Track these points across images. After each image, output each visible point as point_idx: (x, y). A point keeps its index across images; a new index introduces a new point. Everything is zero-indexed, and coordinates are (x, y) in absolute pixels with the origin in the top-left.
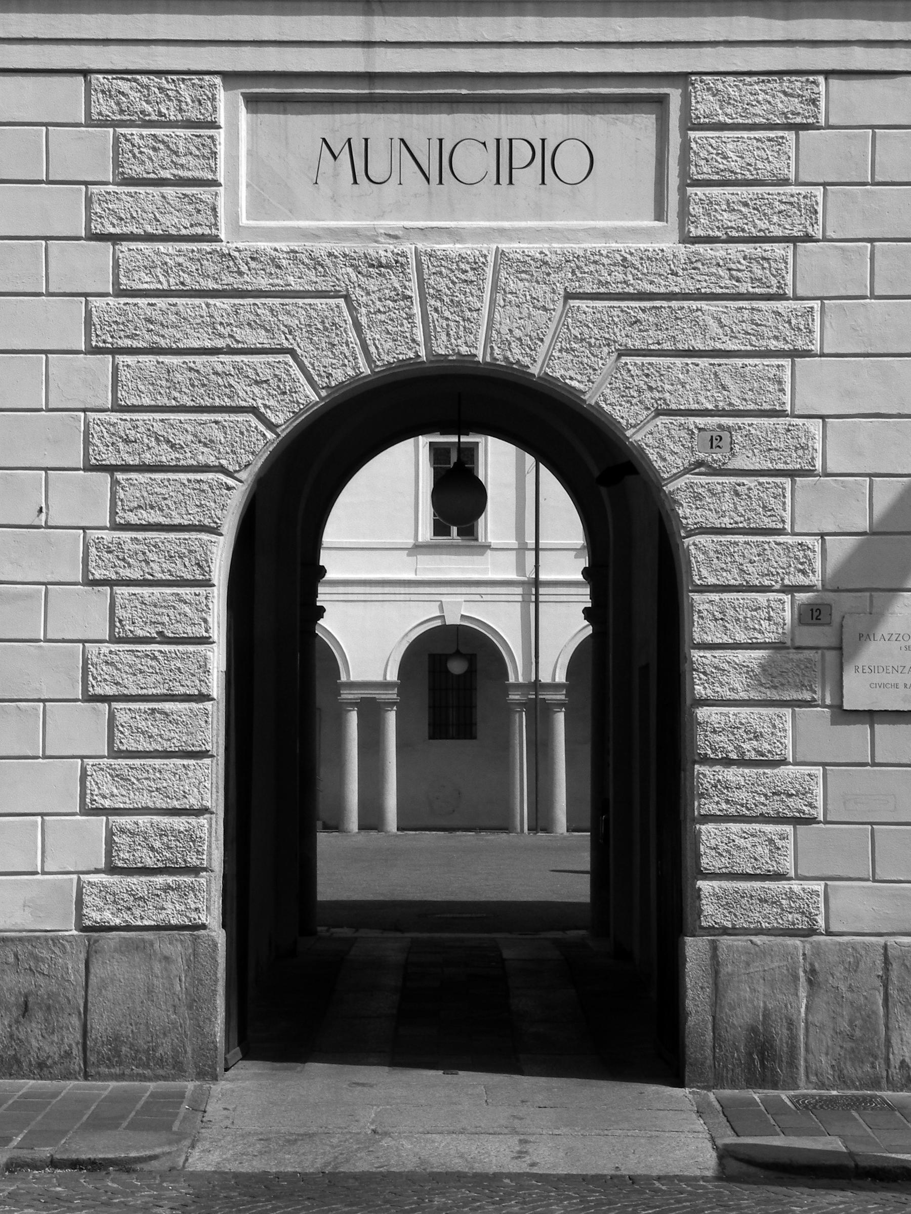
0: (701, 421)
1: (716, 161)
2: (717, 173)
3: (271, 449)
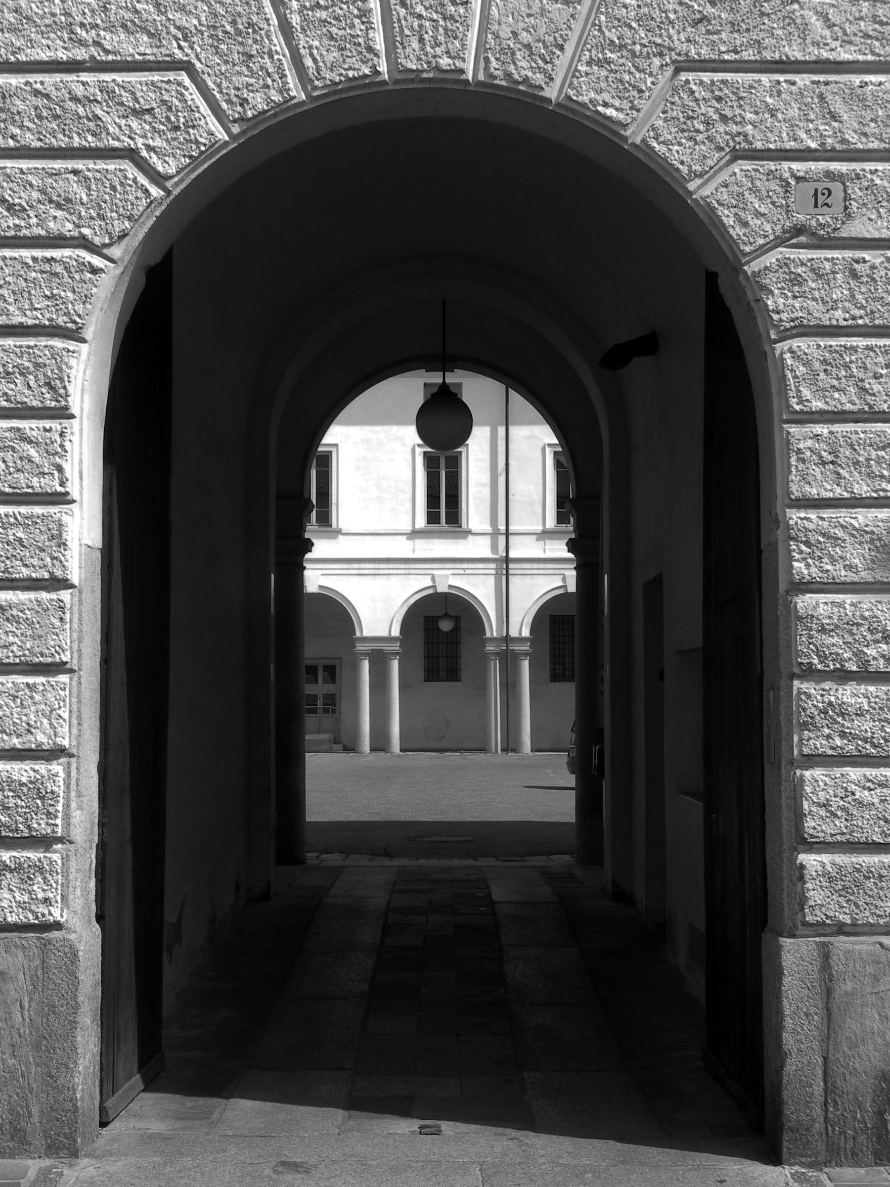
3: (158, 213)
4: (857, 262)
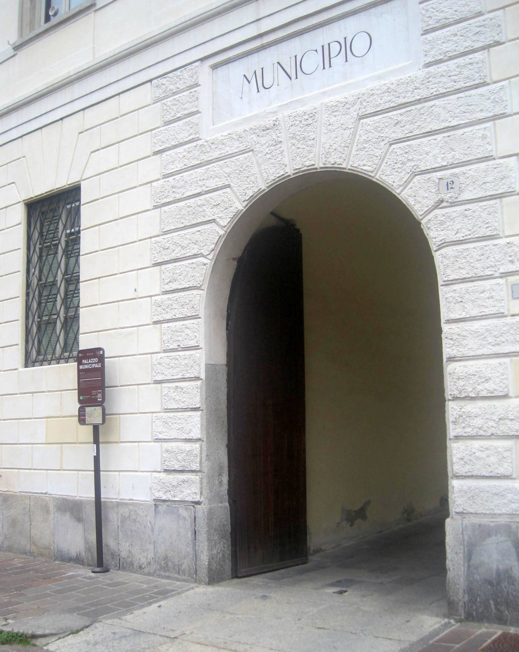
0: (439, 174)
1: (436, 16)
2: (437, 22)
3: (223, 240)
4: (466, 210)
